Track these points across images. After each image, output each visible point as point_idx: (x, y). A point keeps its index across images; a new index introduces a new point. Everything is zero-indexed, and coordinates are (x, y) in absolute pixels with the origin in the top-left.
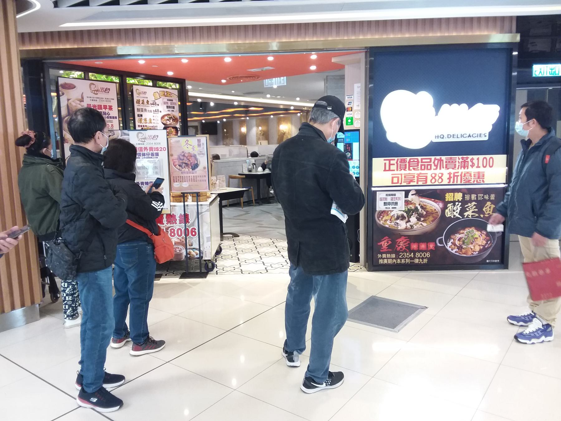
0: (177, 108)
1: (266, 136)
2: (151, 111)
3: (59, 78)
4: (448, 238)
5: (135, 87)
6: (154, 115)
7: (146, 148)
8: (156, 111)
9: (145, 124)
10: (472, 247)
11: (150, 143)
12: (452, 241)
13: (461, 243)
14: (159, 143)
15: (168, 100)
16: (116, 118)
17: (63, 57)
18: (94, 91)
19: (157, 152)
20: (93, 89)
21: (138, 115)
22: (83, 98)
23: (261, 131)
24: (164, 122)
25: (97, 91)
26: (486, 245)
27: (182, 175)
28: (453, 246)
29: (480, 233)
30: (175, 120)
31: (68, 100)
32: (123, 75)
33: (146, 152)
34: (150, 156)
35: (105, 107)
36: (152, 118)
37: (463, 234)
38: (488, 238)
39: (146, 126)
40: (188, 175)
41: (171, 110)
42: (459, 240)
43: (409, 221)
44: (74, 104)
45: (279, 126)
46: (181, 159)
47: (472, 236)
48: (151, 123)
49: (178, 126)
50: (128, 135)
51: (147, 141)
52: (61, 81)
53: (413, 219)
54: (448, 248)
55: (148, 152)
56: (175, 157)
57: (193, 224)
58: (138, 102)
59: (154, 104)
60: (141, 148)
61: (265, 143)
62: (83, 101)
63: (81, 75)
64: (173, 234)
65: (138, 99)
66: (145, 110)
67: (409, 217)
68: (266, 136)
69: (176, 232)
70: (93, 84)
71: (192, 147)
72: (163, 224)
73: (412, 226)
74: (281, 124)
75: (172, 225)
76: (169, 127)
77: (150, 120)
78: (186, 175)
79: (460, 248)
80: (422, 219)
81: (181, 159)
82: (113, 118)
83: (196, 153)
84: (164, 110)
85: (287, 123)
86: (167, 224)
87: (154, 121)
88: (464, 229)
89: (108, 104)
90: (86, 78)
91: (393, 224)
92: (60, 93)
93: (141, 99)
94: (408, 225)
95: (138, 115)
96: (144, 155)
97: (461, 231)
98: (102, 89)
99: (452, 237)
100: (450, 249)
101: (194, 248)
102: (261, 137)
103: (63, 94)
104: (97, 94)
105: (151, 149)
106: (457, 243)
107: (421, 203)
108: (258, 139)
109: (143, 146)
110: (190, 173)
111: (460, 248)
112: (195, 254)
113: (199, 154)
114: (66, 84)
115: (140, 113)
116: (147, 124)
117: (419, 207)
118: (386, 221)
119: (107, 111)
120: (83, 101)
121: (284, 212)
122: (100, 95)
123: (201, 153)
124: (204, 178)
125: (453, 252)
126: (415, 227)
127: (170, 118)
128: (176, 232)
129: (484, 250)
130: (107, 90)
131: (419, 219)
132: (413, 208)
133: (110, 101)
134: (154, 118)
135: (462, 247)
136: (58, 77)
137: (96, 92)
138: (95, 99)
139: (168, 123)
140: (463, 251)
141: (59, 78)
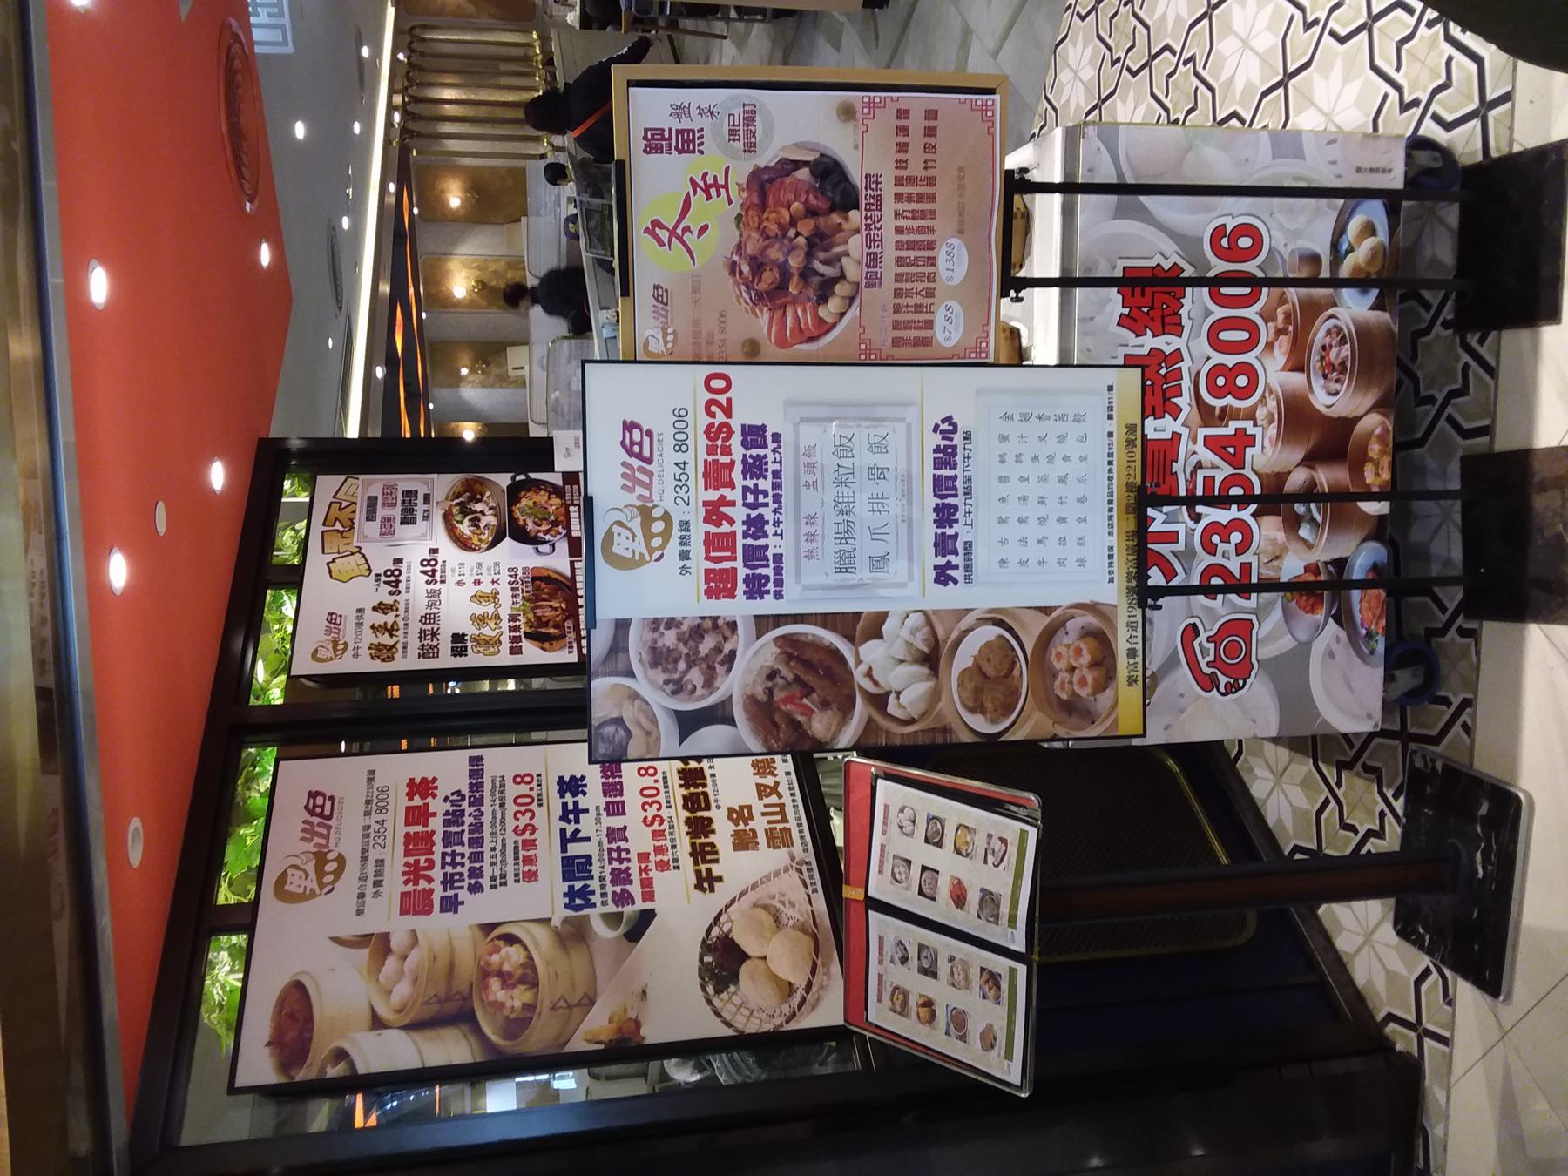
1: (490, 353)
2: (434, 595)
3: (242, 1080)
5: (304, 666)
6: (452, 579)
7: (714, 512)
8: (431, 568)
9: (505, 625)
11: (680, 484)
14: (680, 415)
15: (371, 516)
17: (78, 1074)
18: (320, 873)
19: (736, 441)
20: (312, 883)
23: (472, 370)
24: (487, 536)
25: (321, 858)
27: (889, 284)
30: (472, 492)
31: (377, 1023)
32: (230, 726)
33: (739, 513)
34: (765, 484)
35: (417, 815)
36: (472, 590)
39: (513, 618)
40: (890, 238)
41: (420, 507)
44: (402, 991)
45: (458, 304)
46: (782, 287)
48: (494, 596)
49: (504, 480)
50: (622, 626)
51: (665, 499)
52: (259, 1068)
55: (735, 495)
56: (761, 324)
57: (1185, 241)
59: (393, 578)
60: (711, 542)
61: (516, 356)
62: (385, 938)
63: (232, 949)
64: (1242, 381)
65: (365, 653)
66: (427, 619)
68: (490, 353)
69: (1230, 360)
70: (282, 879)
71: (698, 198)
72: (1176, 436)
74: (450, 296)
75: (1186, 384)
77: (478, 598)
78: (890, 254)
81: (782, 287)
83: (740, 173)
84: (424, 540)
85: (446, 274)
86: (1176, 412)
87: (486, 579)
89: (399, 802)
90: (244, 919)
92: (333, 1072)
93: (369, 638)
95: (459, 652)
96: (756, 526)
98: (309, 832)
101: (1335, 246)
102: (495, 370)
103: (341, 1055)
104: (341, 860)
105: (716, 475)
108: (503, 380)
109: (699, 530)
110: (874, 223)
112: (1369, 243)
113: (750, 148)
115: (445, 644)
119: (438, 806)
120: (385, 938)
123: (744, 131)
124: (917, 123)
127: (465, 511)
128: (1230, 360)
130: (319, 807)
133: (383, 790)
134: (469, 580)
136: (233, 1090)
137: (327, 867)
138: (371, 868)
139: (489, 519)
141: (242, 1080)
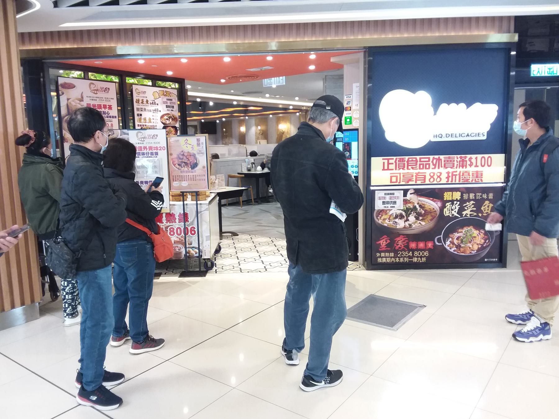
0: (176, 107)
1: (265, 135)
2: (150, 111)
3: (59, 78)
4: (446, 237)
5: (134, 87)
6: (154, 114)
7: (145, 148)
8: (156, 111)
9: (144, 124)
10: (471, 246)
11: (149, 143)
12: (450, 239)
13: (459, 242)
14: (159, 143)
15: (167, 100)
16: (116, 117)
17: (63, 56)
18: (94, 90)
19: (156, 151)
20: (93, 89)
21: (138, 115)
22: (82, 97)
23: (260, 130)
24: (164, 122)
25: (97, 90)
26: (484, 244)
27: (181, 174)
28: (451, 245)
29: (478, 231)
30: (174, 119)
31: (68, 99)
32: (122, 74)
33: (145, 151)
34: (150, 155)
35: (105, 107)
36: (152, 118)
37: (461, 233)
38: (486, 237)
39: (146, 125)
40: (187, 174)
41: (170, 109)
42: (457, 239)
43: (407, 220)
44: (73, 104)
45: (278, 125)
46: (180, 159)
47: (470, 235)
48: (150, 122)
49: (177, 125)
50: (128, 134)
51: (146, 140)
52: (61, 81)
53: (412, 218)
54: (446, 247)
55: (148, 151)
56: (175, 156)
57: (192, 223)
58: (138, 101)
59: (153, 103)
60: (141, 147)
61: (264, 142)
62: (83, 101)
63: (81, 75)
64: (172, 233)
65: (137, 98)
66: (145, 109)
67: (408, 216)
68: (265, 135)
69: (175, 231)
70: (93, 84)
71: (191, 146)
72: (163, 223)
73: (410, 225)
74: (280, 123)
75: (171, 224)
76: (168, 127)
77: (150, 119)
78: (185, 174)
79: (458, 247)
80: (421, 218)
81: (180, 159)
82: (113, 117)
83: (195, 152)
84: (163, 110)
85: (286, 122)
86: (167, 223)
87: (154, 121)
88: (462, 228)
89: (107, 104)
90: (86, 78)
91: (391, 223)
92: (60, 92)
93: (141, 99)
94: (407, 224)
95: (138, 115)
96: (143, 154)
97: (460, 230)
98: (102, 88)
99: (451, 236)
100: (448, 248)
101: (193, 247)
102: (260, 136)
103: (63, 94)
104: (97, 93)
105: (151, 148)
106: (456, 242)
107: (420, 202)
108: (257, 138)
109: (142, 145)
110: (189, 172)
111: (458, 247)
112: (194, 253)
113: (198, 153)
114: (65, 83)
115: (140, 113)
116: (147, 124)
117: (417, 206)
118: (384, 220)
119: (107, 110)
120: (83, 101)
121: (283, 211)
122: (100, 95)
123: (200, 153)
124: (203, 178)
125: (452, 250)
126: (414, 226)
127: (169, 117)
128: (175, 231)
129: (482, 248)
130: (107, 90)
131: (417, 218)
132: (412, 207)
133: (110, 101)
134: (154, 117)
135: (460, 246)
136: (58, 77)
137: (96, 91)
138: (95, 99)
139: (168, 122)
140: (462, 249)
141: (59, 78)
